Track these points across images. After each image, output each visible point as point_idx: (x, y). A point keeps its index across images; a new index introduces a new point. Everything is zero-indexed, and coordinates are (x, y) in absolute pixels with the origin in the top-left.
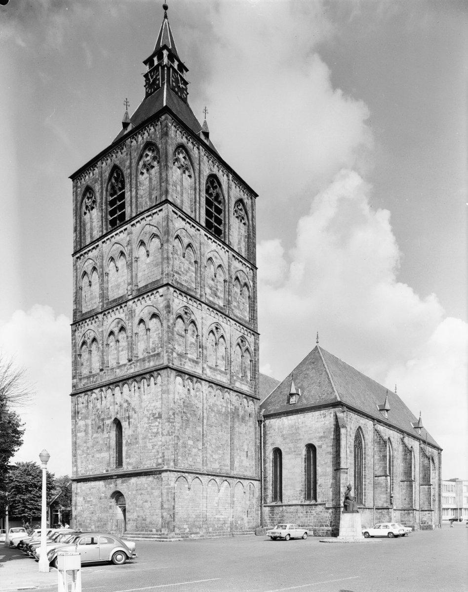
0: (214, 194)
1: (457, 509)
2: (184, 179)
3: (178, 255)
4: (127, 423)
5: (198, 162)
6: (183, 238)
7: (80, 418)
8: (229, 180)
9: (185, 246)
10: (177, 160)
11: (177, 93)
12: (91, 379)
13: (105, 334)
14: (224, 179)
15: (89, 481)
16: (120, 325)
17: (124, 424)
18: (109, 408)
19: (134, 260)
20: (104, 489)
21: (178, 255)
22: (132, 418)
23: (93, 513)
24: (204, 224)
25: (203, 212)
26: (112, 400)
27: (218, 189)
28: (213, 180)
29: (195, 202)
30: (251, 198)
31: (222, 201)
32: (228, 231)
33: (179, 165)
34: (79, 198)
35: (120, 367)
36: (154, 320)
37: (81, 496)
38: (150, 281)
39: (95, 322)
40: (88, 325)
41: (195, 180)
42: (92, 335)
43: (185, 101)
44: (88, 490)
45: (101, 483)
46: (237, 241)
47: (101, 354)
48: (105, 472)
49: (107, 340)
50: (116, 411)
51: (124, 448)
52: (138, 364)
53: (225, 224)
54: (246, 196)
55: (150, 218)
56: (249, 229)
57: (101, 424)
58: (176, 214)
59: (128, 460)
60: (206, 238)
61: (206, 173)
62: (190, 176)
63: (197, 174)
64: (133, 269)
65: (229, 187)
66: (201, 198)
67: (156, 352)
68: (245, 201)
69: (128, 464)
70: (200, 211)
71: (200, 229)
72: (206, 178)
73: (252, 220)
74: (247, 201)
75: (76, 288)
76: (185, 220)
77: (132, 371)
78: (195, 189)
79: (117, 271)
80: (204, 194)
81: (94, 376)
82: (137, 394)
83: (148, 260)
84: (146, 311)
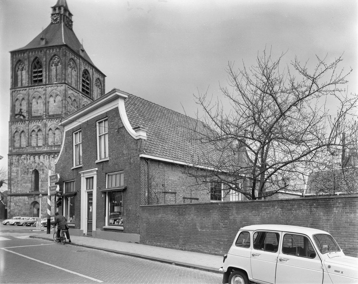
0: (86, 77)
1: (286, 251)
2: (72, 72)
3: (69, 104)
4: (42, 172)
5: (79, 65)
6: (72, 97)
7: (13, 166)
8: (93, 71)
9: (73, 100)
10: (70, 64)
11: (68, 27)
12: (21, 149)
13: (29, 131)
14: (90, 71)
15: (18, 196)
16: (38, 129)
17: (40, 173)
18: (31, 164)
19: (47, 102)
20: (28, 200)
21: (69, 104)
22: (45, 170)
23: (20, 211)
24: (81, 91)
25: (81, 86)
26: (33, 161)
27: (88, 75)
28: (86, 72)
29: (77, 81)
30: (103, 77)
31: (90, 80)
32: (92, 93)
33: (71, 67)
34: (15, 63)
35: (38, 146)
36: (57, 130)
37: (13, 203)
38: (56, 113)
39: (24, 124)
40: (19, 124)
41: (78, 72)
42: (22, 129)
43: (71, 30)
44: (18, 200)
45: (26, 197)
46: (96, 96)
47: (27, 139)
48: (28, 192)
49: (31, 133)
50: (36, 166)
51: (40, 183)
52: (49, 147)
53: (91, 94)
54: (101, 77)
55: (56, 87)
56: (102, 90)
57: (27, 171)
58: (69, 88)
59: (42, 188)
60: (82, 97)
61: (83, 69)
62: (75, 71)
63: (78, 70)
64: (47, 106)
65: (93, 74)
66: (80, 80)
67: (58, 144)
68: (100, 79)
69: (42, 190)
70: (79, 86)
71: (80, 93)
72: (82, 71)
73: (103, 87)
74: (101, 79)
75: (12, 105)
76: (73, 90)
77: (45, 150)
78: (77, 76)
79: (37, 104)
80: (81, 78)
81: (22, 148)
82: (48, 160)
83: (55, 104)
84: (53, 126)
